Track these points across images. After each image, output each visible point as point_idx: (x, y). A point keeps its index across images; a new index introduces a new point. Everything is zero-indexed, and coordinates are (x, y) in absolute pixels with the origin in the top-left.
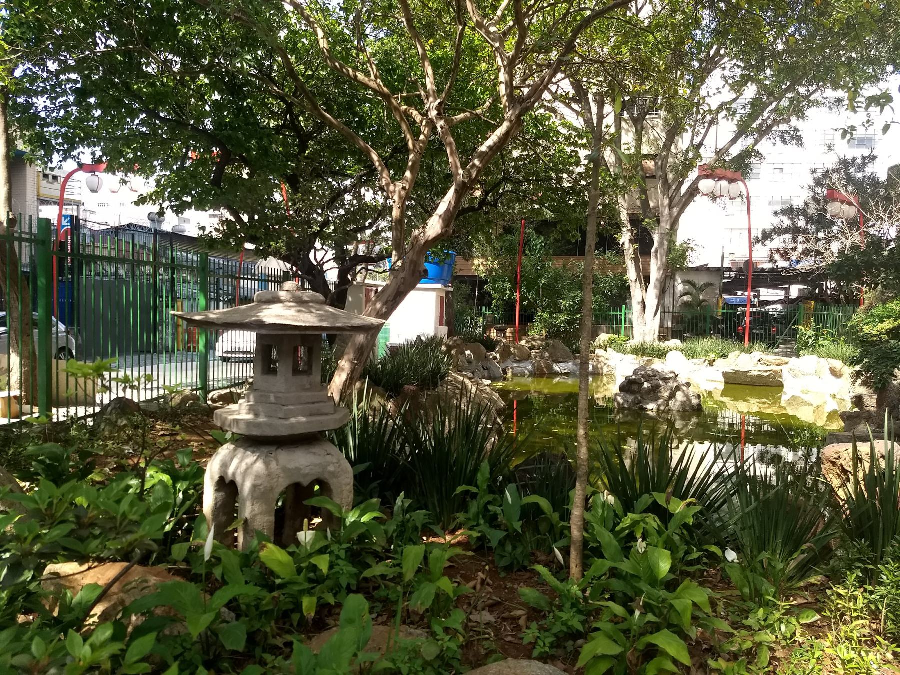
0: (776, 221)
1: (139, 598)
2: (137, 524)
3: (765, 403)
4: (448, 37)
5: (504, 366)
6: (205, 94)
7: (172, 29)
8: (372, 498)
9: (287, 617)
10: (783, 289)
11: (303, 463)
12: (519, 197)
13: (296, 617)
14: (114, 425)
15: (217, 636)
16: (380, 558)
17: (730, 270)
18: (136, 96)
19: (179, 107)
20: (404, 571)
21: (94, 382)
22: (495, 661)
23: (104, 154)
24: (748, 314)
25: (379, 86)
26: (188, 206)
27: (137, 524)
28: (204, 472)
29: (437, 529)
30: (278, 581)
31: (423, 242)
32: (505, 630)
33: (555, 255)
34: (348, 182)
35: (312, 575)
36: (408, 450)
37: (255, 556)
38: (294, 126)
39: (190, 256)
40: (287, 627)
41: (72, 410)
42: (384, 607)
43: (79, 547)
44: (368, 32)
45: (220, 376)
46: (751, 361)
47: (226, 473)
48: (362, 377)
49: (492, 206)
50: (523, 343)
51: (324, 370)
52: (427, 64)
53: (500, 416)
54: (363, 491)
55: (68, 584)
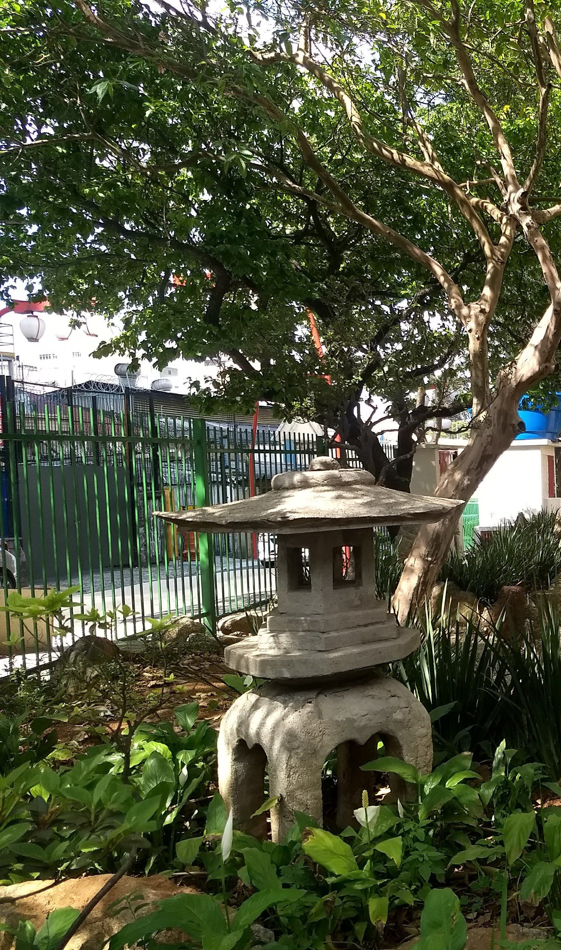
1: (131, 921)
2: (118, 815)
4: (531, 100)
6: (189, 193)
7: (136, 106)
8: (461, 751)
14: (79, 677)
16: (475, 836)
18: (89, 204)
19: (152, 213)
21: (47, 621)
23: (46, 286)
25: (437, 172)
26: (172, 354)
27: (118, 815)
28: (216, 734)
30: (330, 880)
31: (514, 384)
34: (403, 304)
35: (381, 868)
36: (508, 679)
37: (295, 847)
38: (320, 231)
39: (179, 422)
41: (18, 661)
42: (485, 902)
43: (40, 854)
44: (418, 97)
45: (233, 594)
47: (247, 734)
48: (440, 580)
51: (385, 573)
52: (501, 140)
54: (446, 739)
55: (27, 913)
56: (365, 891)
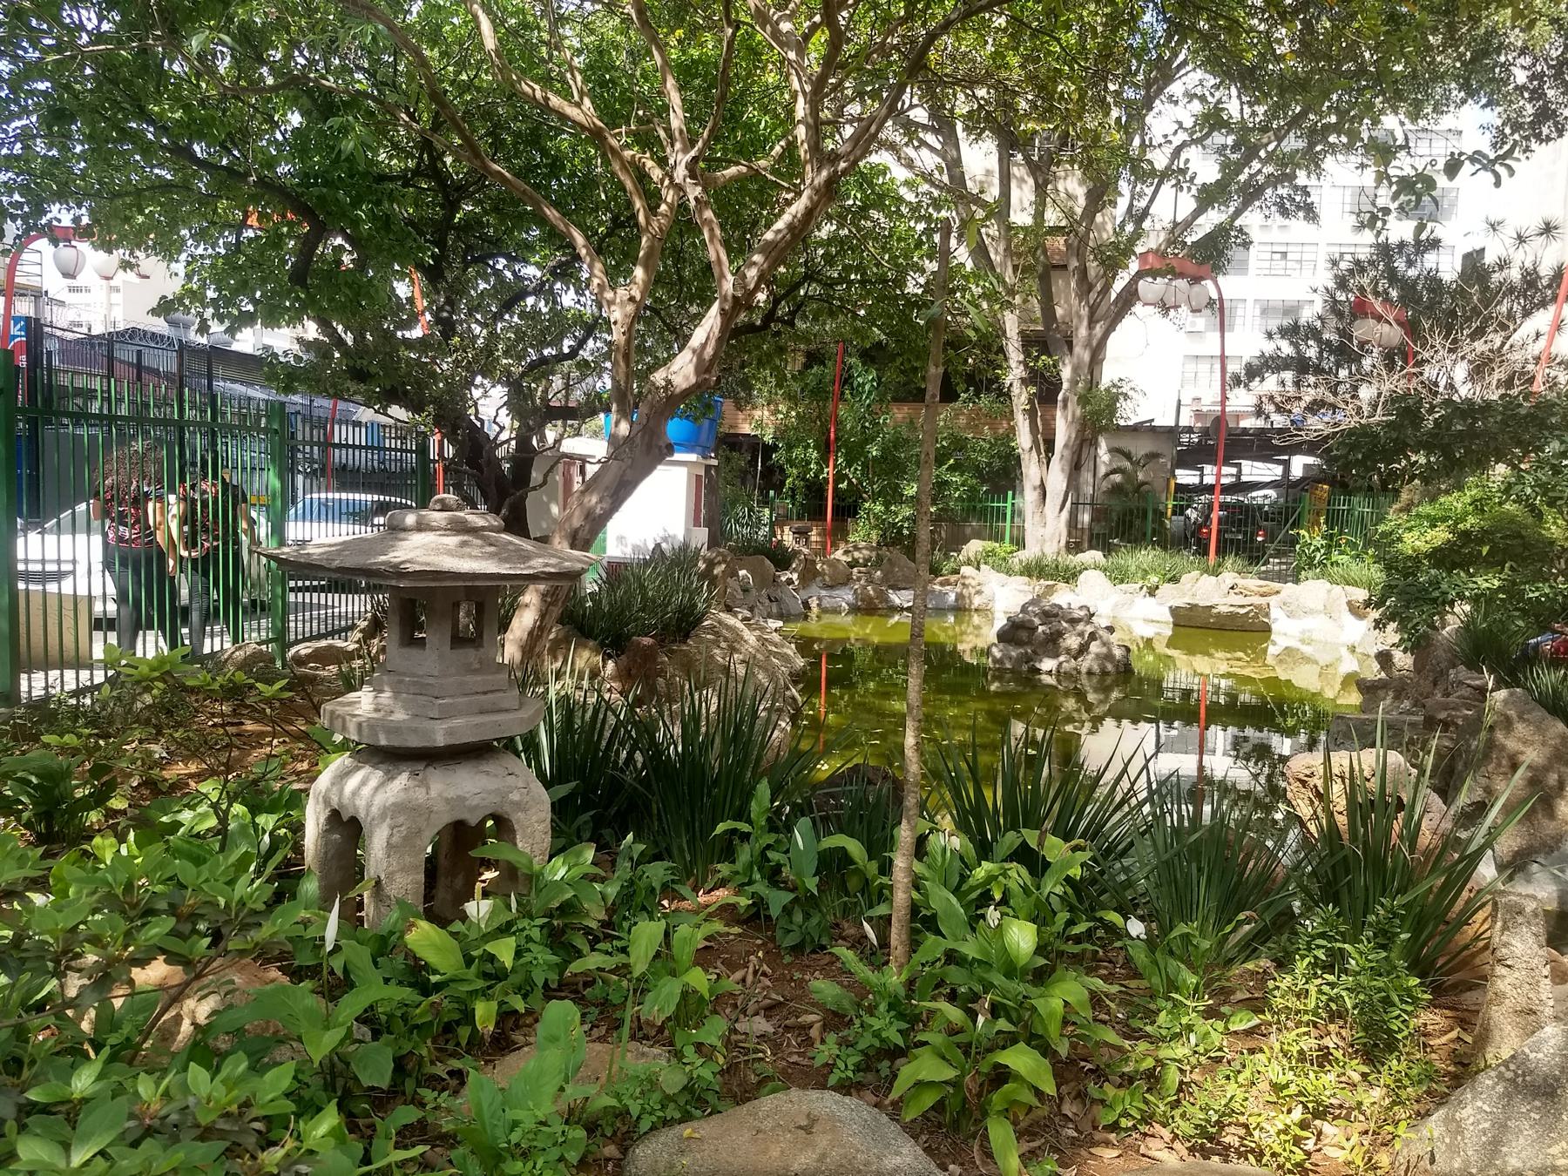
0: (1269, 348)
3: (1239, 659)
5: (803, 595)
9: (450, 1030)
10: (1279, 462)
11: (467, 790)
12: (829, 307)
13: (464, 1033)
15: (348, 1064)
17: (1190, 430)
20: (632, 960)
22: (774, 1091)
24: (1216, 506)
29: (685, 890)
30: (434, 979)
32: (789, 1045)
33: (895, 400)
34: (531, 271)
35: (489, 967)
38: (434, 171)
40: (450, 1047)
42: (601, 1013)
46: (1218, 588)
49: (784, 322)
50: (839, 554)
53: (795, 683)
56: (471, 993)
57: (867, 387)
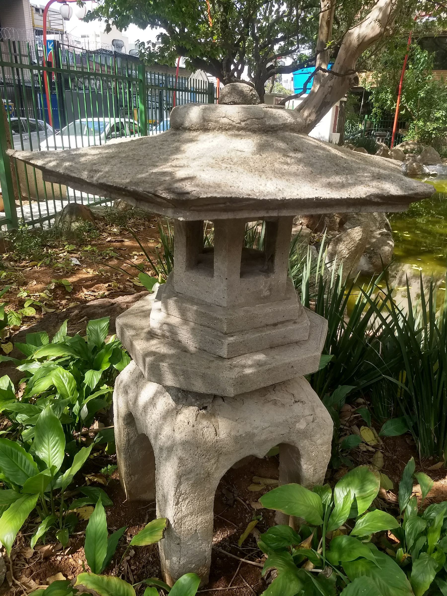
57: (422, 60)
